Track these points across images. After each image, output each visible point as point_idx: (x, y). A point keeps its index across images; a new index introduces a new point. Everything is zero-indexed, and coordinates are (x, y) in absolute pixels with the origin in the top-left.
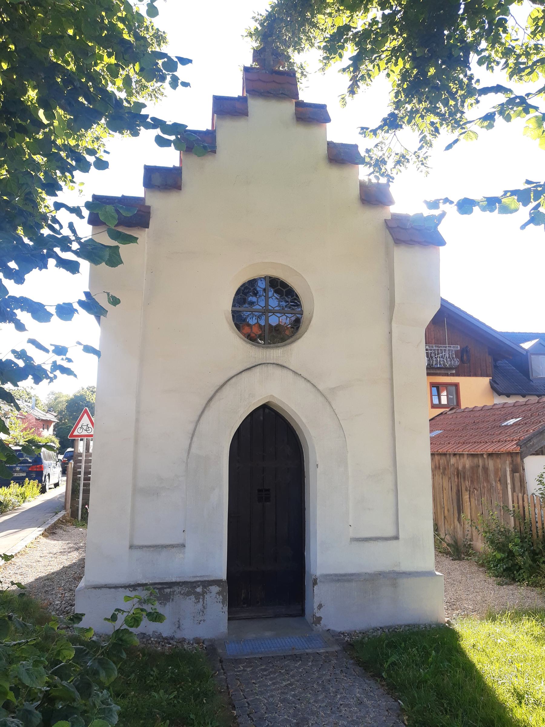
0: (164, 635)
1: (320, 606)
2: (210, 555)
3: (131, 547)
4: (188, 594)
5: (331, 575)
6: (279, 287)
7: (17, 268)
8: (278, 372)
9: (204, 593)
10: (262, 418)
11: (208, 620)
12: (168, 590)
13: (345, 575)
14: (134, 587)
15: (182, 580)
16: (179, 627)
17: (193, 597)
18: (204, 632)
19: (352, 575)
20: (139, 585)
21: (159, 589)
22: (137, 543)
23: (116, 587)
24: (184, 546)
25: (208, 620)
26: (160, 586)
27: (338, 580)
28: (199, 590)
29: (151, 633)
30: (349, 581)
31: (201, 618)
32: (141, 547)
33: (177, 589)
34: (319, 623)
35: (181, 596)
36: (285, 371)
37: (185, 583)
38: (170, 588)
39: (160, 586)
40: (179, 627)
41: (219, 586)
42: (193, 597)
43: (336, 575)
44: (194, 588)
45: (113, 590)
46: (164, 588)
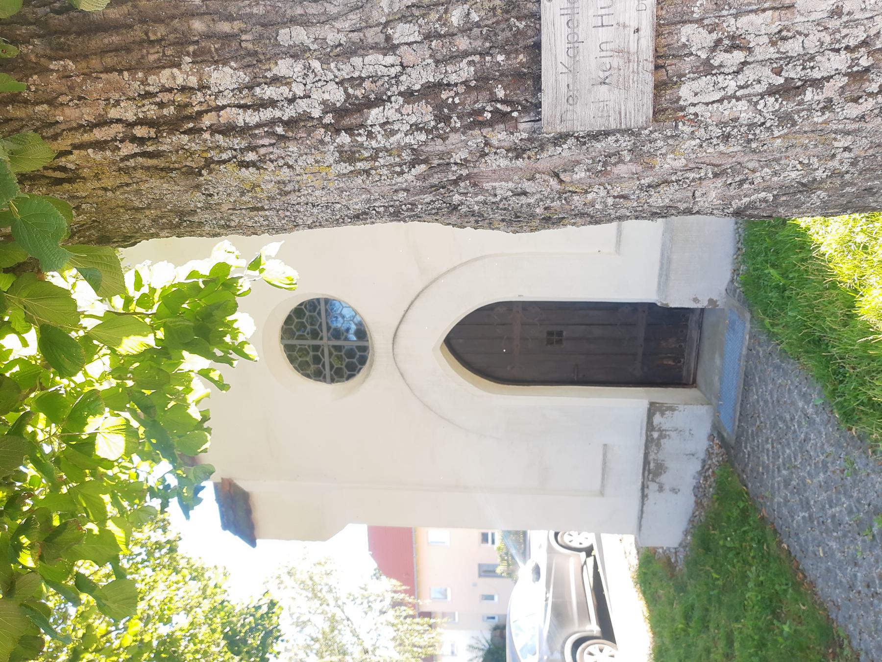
0: (699, 468)
1: (696, 300)
2: (619, 410)
3: (602, 493)
4: (658, 445)
5: (659, 284)
6: (296, 320)
7: (294, 274)
8: (402, 340)
9: (660, 430)
10: (461, 341)
11: (690, 419)
12: (652, 465)
13: (662, 264)
14: (644, 496)
15: (643, 447)
16: (693, 455)
17: (662, 441)
18: (703, 430)
19: (662, 255)
20: (643, 489)
21: (649, 473)
22: (597, 486)
23: (642, 511)
24: (605, 445)
25: (690, 419)
26: (646, 473)
27: (667, 276)
28: (655, 435)
29: (695, 481)
30: (669, 261)
31: (687, 433)
32: (603, 485)
33: (652, 457)
34: (716, 301)
35: (660, 452)
36: (400, 333)
37: (647, 447)
38: (649, 463)
39: (646, 473)
40: (693, 455)
41: (654, 414)
42: (662, 441)
43: (660, 275)
44: (653, 437)
45: (644, 515)
46: (649, 470)
